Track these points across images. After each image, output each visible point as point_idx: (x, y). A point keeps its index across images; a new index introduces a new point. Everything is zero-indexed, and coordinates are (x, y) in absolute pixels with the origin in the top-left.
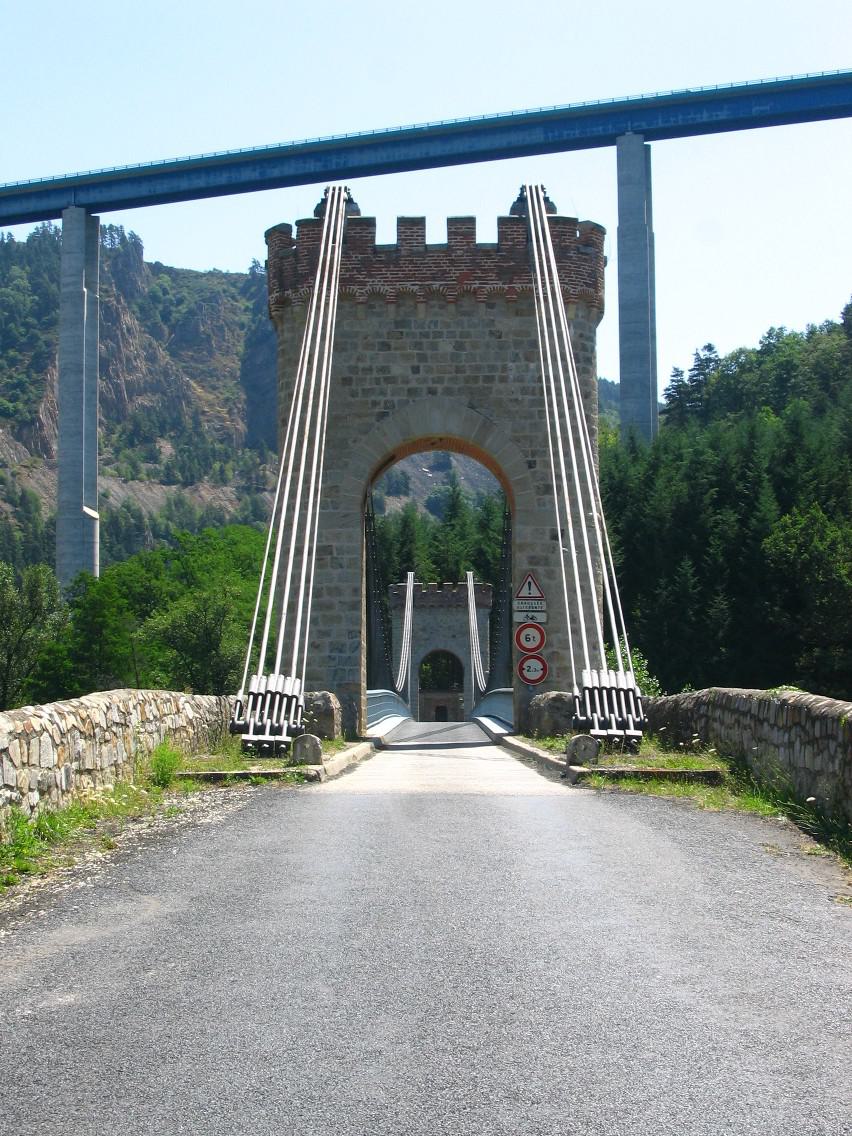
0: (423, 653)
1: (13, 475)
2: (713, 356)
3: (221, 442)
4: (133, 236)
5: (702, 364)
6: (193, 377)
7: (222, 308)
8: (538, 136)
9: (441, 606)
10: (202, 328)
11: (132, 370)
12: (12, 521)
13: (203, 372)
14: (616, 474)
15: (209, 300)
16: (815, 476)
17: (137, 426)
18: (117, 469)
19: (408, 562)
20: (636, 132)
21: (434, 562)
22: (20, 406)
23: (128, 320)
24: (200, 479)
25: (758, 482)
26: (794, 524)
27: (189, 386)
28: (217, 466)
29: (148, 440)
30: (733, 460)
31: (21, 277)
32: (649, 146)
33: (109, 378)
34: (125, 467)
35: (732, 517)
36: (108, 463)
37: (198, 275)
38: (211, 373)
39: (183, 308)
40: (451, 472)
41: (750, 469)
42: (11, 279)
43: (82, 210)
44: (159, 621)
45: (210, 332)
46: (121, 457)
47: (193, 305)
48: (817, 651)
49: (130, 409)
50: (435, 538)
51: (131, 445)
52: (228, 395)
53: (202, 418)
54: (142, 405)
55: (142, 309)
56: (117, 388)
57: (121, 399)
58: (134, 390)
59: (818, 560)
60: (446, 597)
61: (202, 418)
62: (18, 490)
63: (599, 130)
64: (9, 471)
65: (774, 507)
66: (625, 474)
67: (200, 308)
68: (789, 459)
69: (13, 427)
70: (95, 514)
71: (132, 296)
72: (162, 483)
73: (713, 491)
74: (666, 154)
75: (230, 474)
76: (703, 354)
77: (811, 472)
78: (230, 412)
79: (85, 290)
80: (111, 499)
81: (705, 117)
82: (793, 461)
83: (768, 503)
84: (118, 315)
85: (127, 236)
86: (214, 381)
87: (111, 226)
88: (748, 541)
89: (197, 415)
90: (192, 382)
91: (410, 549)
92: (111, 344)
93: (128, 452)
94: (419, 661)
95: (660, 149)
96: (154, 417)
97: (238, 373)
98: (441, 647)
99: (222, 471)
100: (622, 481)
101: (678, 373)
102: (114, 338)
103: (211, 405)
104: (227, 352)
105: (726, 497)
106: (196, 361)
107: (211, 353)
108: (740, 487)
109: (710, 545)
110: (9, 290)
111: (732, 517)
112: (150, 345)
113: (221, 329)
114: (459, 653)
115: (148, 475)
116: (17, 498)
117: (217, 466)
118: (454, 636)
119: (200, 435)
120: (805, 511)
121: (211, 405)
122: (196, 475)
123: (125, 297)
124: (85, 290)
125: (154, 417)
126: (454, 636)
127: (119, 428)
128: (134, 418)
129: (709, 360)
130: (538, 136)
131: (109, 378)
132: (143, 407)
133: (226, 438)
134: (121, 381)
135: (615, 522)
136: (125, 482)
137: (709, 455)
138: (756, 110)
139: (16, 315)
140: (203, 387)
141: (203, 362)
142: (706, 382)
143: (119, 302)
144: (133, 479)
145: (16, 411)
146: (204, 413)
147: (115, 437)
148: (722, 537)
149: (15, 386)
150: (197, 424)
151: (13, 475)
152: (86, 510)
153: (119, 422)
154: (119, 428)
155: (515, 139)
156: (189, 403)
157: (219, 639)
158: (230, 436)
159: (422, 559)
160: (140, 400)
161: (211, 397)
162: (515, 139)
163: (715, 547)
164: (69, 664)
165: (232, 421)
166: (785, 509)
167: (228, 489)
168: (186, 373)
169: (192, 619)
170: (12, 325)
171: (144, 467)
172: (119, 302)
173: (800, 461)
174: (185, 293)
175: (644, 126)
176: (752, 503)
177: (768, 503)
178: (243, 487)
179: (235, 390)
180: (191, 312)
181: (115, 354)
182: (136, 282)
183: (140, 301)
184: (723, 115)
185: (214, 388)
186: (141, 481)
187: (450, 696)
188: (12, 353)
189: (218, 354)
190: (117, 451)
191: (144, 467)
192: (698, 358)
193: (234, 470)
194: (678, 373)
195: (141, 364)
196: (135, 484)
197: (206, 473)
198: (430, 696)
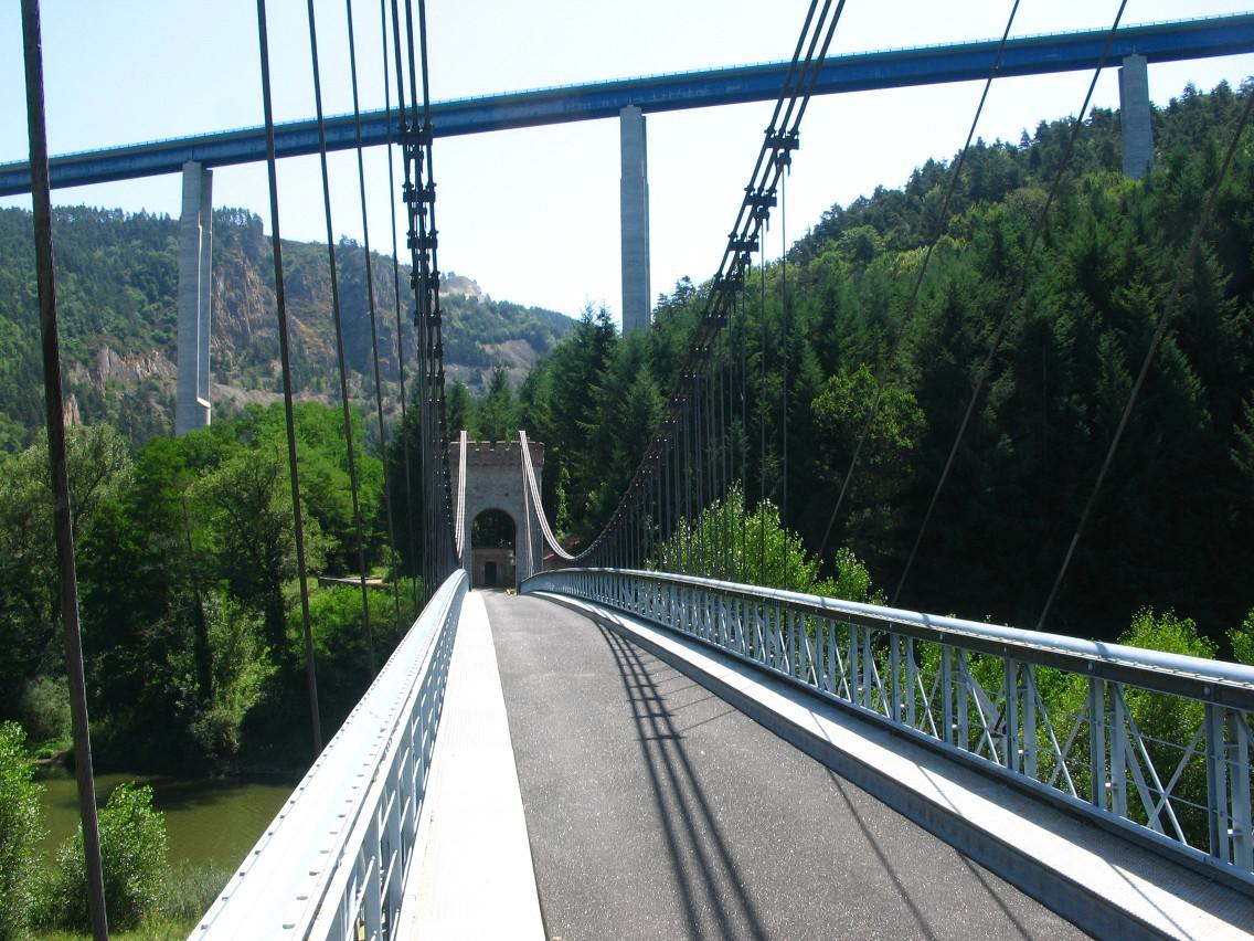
0: (476, 511)
1: (165, 385)
2: (689, 285)
3: (318, 362)
4: (256, 216)
5: (682, 291)
6: (298, 316)
7: (319, 268)
8: (558, 108)
9: (495, 465)
10: (305, 283)
11: (254, 310)
12: (163, 418)
13: (305, 313)
14: (660, 340)
15: (310, 263)
16: (853, 343)
17: (257, 350)
18: (242, 382)
19: (459, 425)
20: (636, 105)
21: (481, 430)
22: (172, 335)
23: (251, 275)
24: (302, 389)
25: (799, 347)
26: (843, 384)
27: (295, 324)
28: (314, 380)
29: (265, 361)
30: (774, 327)
31: (174, 244)
32: (645, 118)
33: (237, 316)
34: (248, 380)
35: (775, 379)
36: (235, 377)
37: (303, 245)
38: (312, 314)
39: (292, 268)
40: (482, 385)
41: (790, 335)
42: (168, 245)
43: (199, 164)
44: (212, 479)
45: (310, 285)
46: (245, 372)
47: (299, 266)
48: (867, 512)
49: (252, 339)
50: (482, 409)
51: (253, 364)
52: (323, 330)
53: (304, 346)
54: (261, 336)
55: (262, 268)
56: (243, 324)
57: (245, 331)
58: (255, 325)
59: (869, 415)
60: (499, 455)
61: (304, 346)
62: (168, 394)
63: (606, 103)
64: (162, 383)
65: (817, 370)
66: (669, 339)
67: (304, 268)
68: (828, 325)
69: (166, 351)
70: (207, 404)
71: (255, 259)
72: (274, 391)
73: (757, 354)
74: (660, 125)
75: (324, 385)
76: (683, 283)
77: (848, 339)
78: (324, 342)
79: (200, 227)
80: (237, 403)
81: (689, 94)
82: (833, 326)
83: (812, 367)
84: (244, 273)
85: (252, 216)
86: (313, 321)
87: (240, 210)
88: (795, 402)
89: (301, 343)
90: (297, 321)
91: (460, 416)
92: (238, 291)
93: (251, 369)
94: (473, 518)
95: (655, 121)
96: (269, 345)
97: (331, 315)
98: (494, 505)
99: (318, 383)
100: (666, 347)
101: (663, 297)
102: (241, 288)
103: (311, 337)
104: (323, 300)
105: (771, 361)
106: (301, 305)
107: (311, 300)
108: (782, 351)
109: (757, 406)
110: (165, 253)
111: (775, 379)
112: (268, 293)
113: (319, 283)
114: (512, 511)
115: (264, 386)
116: (167, 401)
117: (314, 380)
118: (507, 495)
119: (303, 358)
120: (853, 369)
121: (311, 337)
122: (298, 385)
123: (250, 260)
124: (200, 227)
125: (269, 345)
126: (507, 495)
127: (244, 353)
128: (255, 346)
129: (686, 288)
130: (558, 108)
131: (237, 316)
132: (262, 338)
133: (322, 360)
134: (246, 319)
135: (662, 385)
136: (248, 390)
137: (750, 322)
138: (729, 89)
139: (170, 271)
140: (305, 324)
141: (306, 306)
142: (684, 305)
143: (244, 262)
144: (253, 388)
145: (169, 339)
146: (306, 342)
147: (241, 358)
148: (769, 397)
149: (168, 321)
150: (301, 350)
151: (165, 385)
152: (200, 400)
153: (244, 348)
154: (244, 353)
155: (540, 109)
156: (295, 335)
157: (269, 498)
158: (324, 359)
159: (470, 417)
160: (259, 333)
161: (311, 331)
162: (540, 109)
163: (763, 408)
164: (125, 523)
165: (326, 348)
166: (829, 368)
167: (322, 396)
168: (294, 314)
169: (243, 477)
170: (167, 278)
171: (261, 380)
172: (244, 262)
173: (840, 327)
174: (293, 257)
175: (642, 100)
176: (795, 368)
177: (812, 367)
178: (333, 396)
179: (328, 326)
180: (297, 271)
181: (242, 299)
182: (257, 249)
183: (261, 262)
184: (703, 92)
185: (313, 325)
186: (259, 389)
187: (498, 552)
188: (166, 298)
189: (316, 301)
190: (242, 368)
191: (261, 380)
192: (679, 286)
193: (327, 383)
194: (663, 297)
195: (260, 307)
196: (256, 392)
197: (306, 385)
198: (480, 552)
